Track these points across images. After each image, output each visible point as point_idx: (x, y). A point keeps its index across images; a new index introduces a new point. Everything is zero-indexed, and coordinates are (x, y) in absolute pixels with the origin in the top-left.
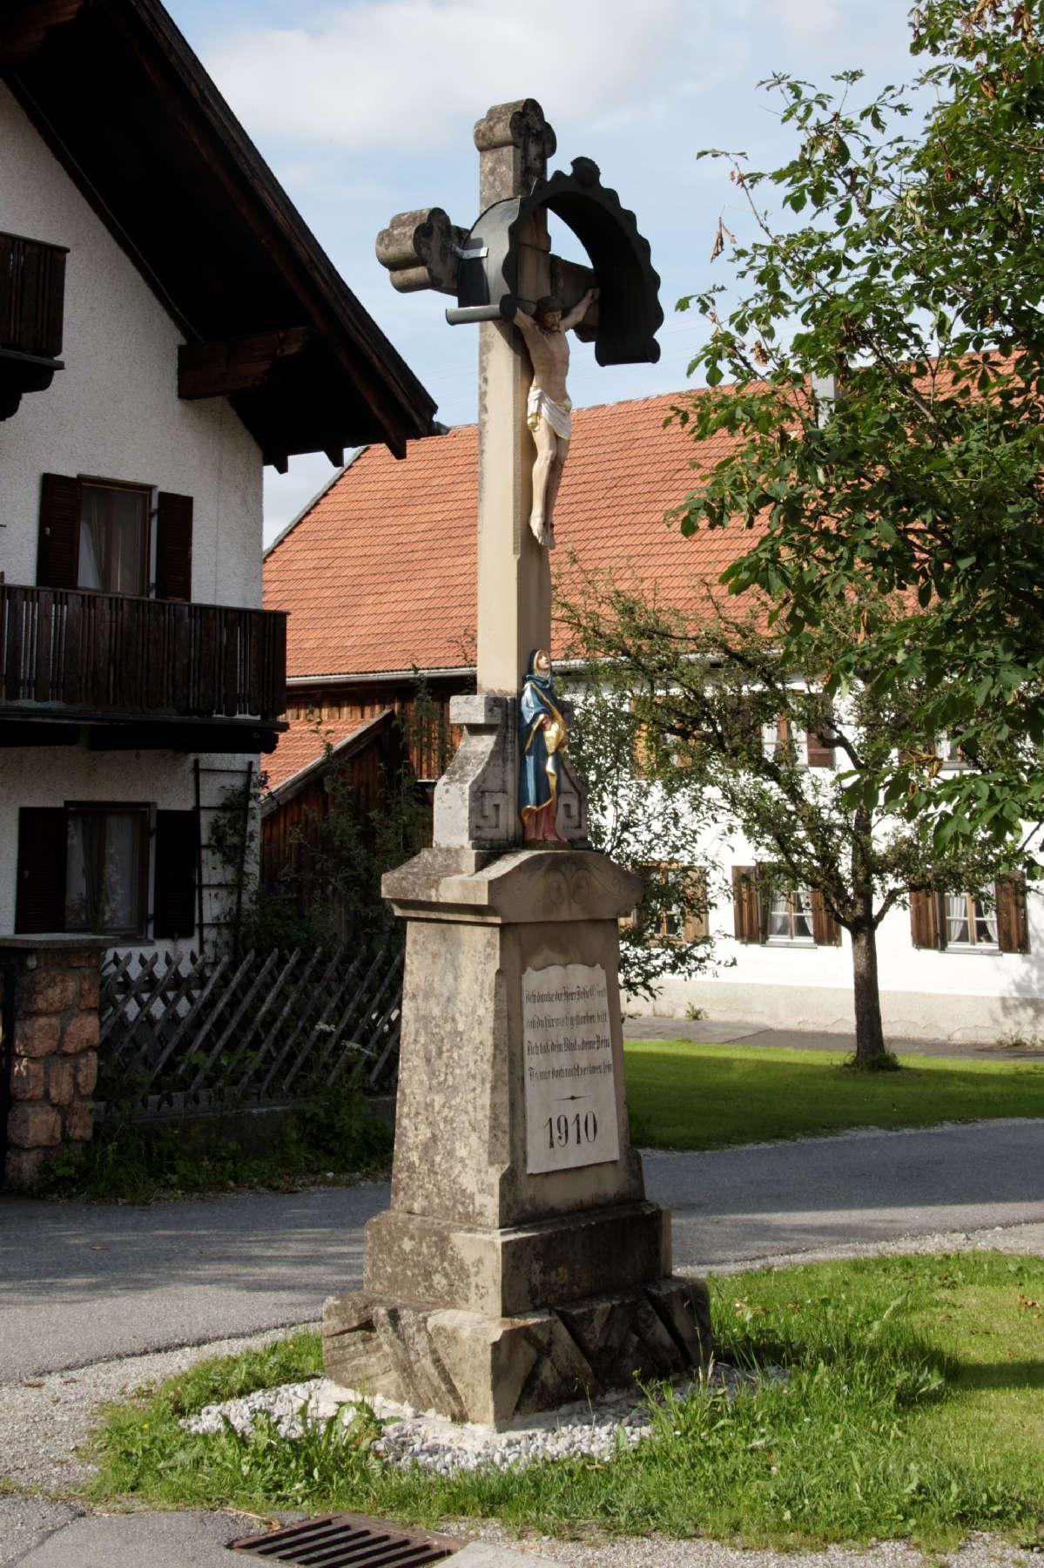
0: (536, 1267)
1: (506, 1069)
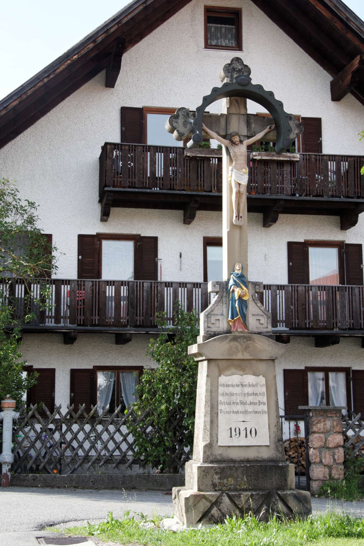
0: (217, 477)
1: (209, 410)
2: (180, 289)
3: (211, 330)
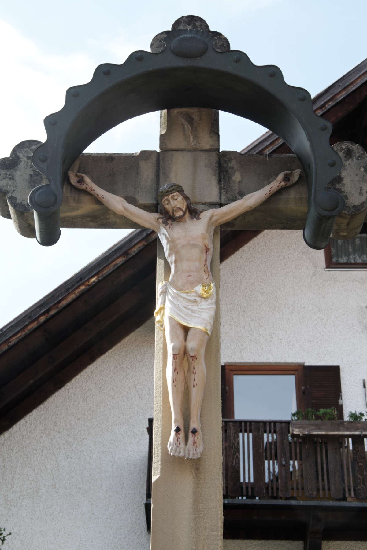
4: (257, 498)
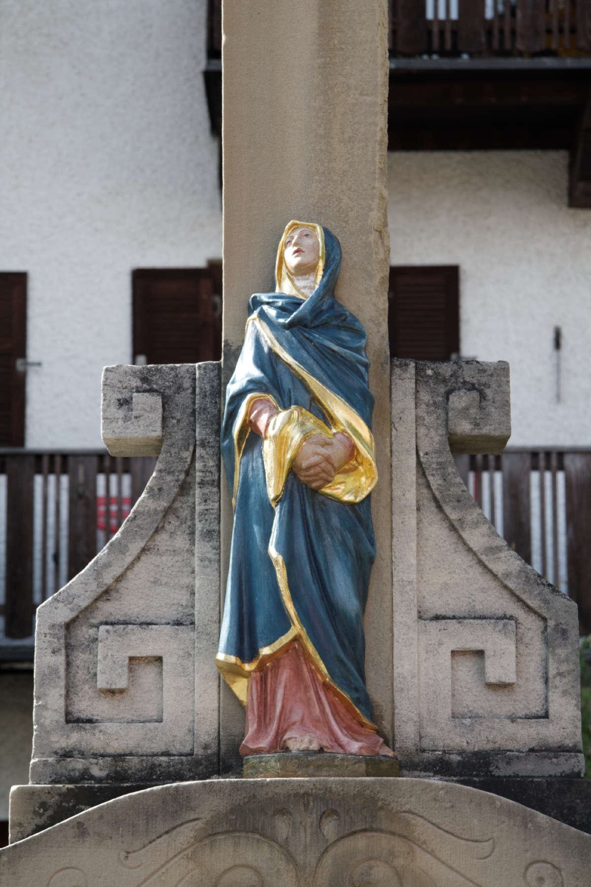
2: (535, 477)
3: (92, 740)
4: (465, 57)
